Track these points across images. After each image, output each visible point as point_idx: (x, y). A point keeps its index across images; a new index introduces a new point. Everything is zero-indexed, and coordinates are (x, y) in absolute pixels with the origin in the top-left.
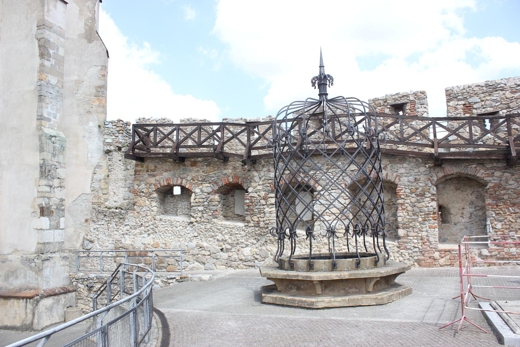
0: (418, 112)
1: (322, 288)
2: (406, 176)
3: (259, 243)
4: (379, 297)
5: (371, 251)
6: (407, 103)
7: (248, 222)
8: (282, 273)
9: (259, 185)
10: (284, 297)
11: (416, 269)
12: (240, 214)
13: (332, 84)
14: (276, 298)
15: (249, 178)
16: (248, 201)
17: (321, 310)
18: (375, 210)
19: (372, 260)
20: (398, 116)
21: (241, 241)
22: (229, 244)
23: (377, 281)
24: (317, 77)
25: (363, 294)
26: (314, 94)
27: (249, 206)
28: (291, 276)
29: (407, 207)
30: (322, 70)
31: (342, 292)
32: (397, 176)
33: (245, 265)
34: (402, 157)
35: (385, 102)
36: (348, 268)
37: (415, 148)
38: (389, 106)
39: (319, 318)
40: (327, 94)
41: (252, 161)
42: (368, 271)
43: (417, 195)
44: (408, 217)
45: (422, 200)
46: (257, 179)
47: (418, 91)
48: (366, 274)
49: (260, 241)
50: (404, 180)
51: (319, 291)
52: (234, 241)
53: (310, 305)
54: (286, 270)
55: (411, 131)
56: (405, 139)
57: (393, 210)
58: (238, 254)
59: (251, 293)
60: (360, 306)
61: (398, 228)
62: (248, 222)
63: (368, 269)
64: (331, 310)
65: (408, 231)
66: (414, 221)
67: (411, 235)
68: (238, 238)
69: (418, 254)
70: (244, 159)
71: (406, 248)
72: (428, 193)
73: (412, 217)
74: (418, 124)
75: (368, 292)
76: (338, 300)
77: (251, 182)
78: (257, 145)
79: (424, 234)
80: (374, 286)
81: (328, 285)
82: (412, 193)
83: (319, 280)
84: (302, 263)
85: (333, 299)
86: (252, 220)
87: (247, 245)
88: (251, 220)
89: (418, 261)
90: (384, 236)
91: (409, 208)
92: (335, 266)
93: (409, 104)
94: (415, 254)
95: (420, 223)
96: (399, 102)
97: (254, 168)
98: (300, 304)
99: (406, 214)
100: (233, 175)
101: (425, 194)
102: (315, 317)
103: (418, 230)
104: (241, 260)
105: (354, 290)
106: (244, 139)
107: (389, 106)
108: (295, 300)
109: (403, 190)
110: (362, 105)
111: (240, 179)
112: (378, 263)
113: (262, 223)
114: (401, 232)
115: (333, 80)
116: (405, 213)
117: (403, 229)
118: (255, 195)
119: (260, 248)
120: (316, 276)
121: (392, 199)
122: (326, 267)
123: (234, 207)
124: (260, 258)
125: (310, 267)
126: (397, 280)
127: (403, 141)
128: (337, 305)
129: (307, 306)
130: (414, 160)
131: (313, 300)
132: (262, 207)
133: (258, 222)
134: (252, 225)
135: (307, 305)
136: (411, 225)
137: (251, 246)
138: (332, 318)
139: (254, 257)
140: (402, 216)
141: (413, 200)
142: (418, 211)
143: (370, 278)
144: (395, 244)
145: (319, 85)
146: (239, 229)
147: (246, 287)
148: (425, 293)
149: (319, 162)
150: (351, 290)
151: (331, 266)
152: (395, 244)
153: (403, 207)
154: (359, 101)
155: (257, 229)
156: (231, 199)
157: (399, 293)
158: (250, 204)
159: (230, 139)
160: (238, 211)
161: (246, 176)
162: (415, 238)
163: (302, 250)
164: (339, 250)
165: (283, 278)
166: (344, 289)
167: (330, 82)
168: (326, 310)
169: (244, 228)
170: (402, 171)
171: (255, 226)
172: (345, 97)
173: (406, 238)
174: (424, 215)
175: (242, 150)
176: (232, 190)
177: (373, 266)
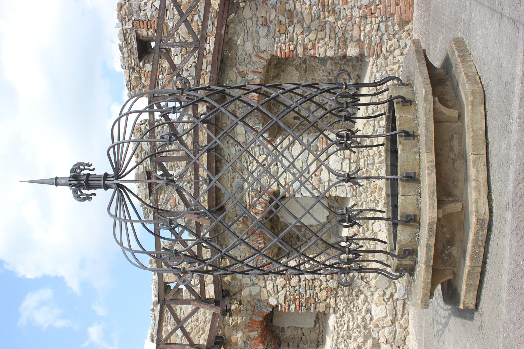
0: (152, 15)
1: (450, 202)
2: (258, 41)
3: (365, 290)
4: (470, 99)
5: (383, 109)
6: (137, 33)
7: (328, 307)
8: (422, 271)
9: (265, 287)
10: (466, 271)
11: (416, 28)
12: (315, 318)
13: (89, 165)
14: (468, 285)
15: (252, 303)
16: (293, 307)
17: (494, 205)
18: (314, 99)
19: (401, 109)
20: (157, 51)
21: (360, 321)
22: (365, 341)
23: (440, 101)
24: (75, 192)
25: (463, 127)
26: (103, 196)
27: (301, 306)
28: (427, 258)
29: (310, 41)
30: (63, 181)
31: (458, 164)
32: (257, 55)
33: (402, 316)
34: (225, 44)
35: (134, 70)
36: (415, 153)
37: (213, 23)
38: (141, 64)
39: (510, 214)
40: (106, 174)
41: (223, 297)
42: (421, 116)
43: (291, 22)
44: (326, 40)
45: (300, 16)
46: (255, 290)
47: (118, 15)
48: (427, 121)
49: (361, 288)
50: (263, 44)
51: (456, 207)
52: (360, 332)
53: (483, 225)
54: (416, 262)
55: (183, 29)
56: (196, 41)
57: (316, 63)
58: (383, 327)
59: (455, 322)
60: (486, 133)
61: (345, 56)
62: (328, 307)
63: (417, 117)
64: (493, 187)
65: (351, 40)
66: (334, 30)
67: (357, 35)
68: (355, 326)
69: (390, 23)
70: (219, 312)
71: (380, 44)
72: (288, 5)
73: (328, 32)
74: (172, 18)
75: (461, 117)
76: (475, 172)
77: (260, 300)
78: (197, 290)
79: (356, 12)
80: (448, 107)
81: (447, 191)
82: (286, 32)
83: (436, 208)
84: (404, 234)
85: (473, 184)
86: (325, 300)
87: (368, 311)
88: (325, 303)
89: (404, 23)
90: (359, 85)
91: (312, 36)
92: (411, 177)
93: (139, 31)
94: (390, 29)
95: (338, 19)
96: (136, 46)
97: (235, 294)
98: (480, 243)
99: (322, 43)
100: (246, 330)
101: (289, 10)
102: (509, 220)
103: (350, 23)
104: (393, 322)
105: (455, 143)
106: (188, 308)
107: (141, 64)
108: (473, 252)
109: (281, 47)
110: (127, 114)
111: (254, 318)
112: (408, 97)
113: (330, 284)
114: (352, 51)
115: (81, 164)
116: (320, 45)
117: (346, 47)
118: (282, 293)
119: (373, 289)
120: (428, 213)
121: (296, 65)
122: (412, 193)
123: (302, 329)
124: (390, 289)
125: (412, 220)
126: (437, 63)
127: (199, 44)
128: (483, 176)
129: (486, 231)
130: (232, 25)
131: (473, 220)
132: (303, 283)
133: (329, 290)
134: (332, 301)
135: (483, 230)
136: (340, 34)
137: (369, 304)
138: (511, 188)
139: (388, 300)
140: (325, 49)
141: (298, 30)
142: (317, 22)
143: (434, 113)
144: (371, 62)
145: (89, 188)
146: (339, 323)
147: (444, 328)
148: (463, 16)
149: (229, 184)
150: (456, 148)
151: (411, 184)
152: (371, 62)
153: (310, 47)
154: (118, 120)
155: (340, 293)
156: (288, 334)
157: (462, 61)
158: (297, 302)
159: (186, 334)
160: (309, 323)
161: (249, 307)
162: (362, 28)
163: (381, 229)
164: (380, 156)
165: (430, 271)
166: (454, 161)
167: (85, 169)
168: (493, 197)
169: (338, 315)
170: (249, 46)
171: (336, 297)
172: (110, 144)
173: (363, 42)
174: (324, 12)
175: (205, 314)
176: (272, 332)
177: (412, 107)
